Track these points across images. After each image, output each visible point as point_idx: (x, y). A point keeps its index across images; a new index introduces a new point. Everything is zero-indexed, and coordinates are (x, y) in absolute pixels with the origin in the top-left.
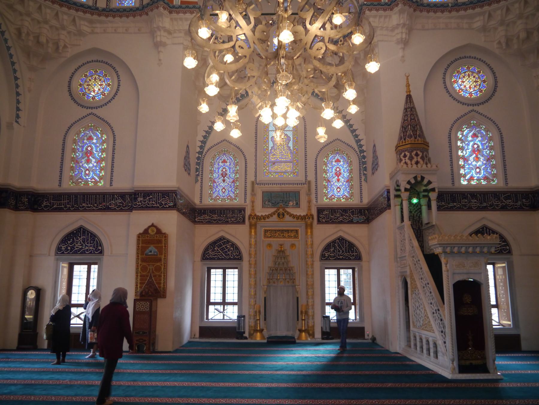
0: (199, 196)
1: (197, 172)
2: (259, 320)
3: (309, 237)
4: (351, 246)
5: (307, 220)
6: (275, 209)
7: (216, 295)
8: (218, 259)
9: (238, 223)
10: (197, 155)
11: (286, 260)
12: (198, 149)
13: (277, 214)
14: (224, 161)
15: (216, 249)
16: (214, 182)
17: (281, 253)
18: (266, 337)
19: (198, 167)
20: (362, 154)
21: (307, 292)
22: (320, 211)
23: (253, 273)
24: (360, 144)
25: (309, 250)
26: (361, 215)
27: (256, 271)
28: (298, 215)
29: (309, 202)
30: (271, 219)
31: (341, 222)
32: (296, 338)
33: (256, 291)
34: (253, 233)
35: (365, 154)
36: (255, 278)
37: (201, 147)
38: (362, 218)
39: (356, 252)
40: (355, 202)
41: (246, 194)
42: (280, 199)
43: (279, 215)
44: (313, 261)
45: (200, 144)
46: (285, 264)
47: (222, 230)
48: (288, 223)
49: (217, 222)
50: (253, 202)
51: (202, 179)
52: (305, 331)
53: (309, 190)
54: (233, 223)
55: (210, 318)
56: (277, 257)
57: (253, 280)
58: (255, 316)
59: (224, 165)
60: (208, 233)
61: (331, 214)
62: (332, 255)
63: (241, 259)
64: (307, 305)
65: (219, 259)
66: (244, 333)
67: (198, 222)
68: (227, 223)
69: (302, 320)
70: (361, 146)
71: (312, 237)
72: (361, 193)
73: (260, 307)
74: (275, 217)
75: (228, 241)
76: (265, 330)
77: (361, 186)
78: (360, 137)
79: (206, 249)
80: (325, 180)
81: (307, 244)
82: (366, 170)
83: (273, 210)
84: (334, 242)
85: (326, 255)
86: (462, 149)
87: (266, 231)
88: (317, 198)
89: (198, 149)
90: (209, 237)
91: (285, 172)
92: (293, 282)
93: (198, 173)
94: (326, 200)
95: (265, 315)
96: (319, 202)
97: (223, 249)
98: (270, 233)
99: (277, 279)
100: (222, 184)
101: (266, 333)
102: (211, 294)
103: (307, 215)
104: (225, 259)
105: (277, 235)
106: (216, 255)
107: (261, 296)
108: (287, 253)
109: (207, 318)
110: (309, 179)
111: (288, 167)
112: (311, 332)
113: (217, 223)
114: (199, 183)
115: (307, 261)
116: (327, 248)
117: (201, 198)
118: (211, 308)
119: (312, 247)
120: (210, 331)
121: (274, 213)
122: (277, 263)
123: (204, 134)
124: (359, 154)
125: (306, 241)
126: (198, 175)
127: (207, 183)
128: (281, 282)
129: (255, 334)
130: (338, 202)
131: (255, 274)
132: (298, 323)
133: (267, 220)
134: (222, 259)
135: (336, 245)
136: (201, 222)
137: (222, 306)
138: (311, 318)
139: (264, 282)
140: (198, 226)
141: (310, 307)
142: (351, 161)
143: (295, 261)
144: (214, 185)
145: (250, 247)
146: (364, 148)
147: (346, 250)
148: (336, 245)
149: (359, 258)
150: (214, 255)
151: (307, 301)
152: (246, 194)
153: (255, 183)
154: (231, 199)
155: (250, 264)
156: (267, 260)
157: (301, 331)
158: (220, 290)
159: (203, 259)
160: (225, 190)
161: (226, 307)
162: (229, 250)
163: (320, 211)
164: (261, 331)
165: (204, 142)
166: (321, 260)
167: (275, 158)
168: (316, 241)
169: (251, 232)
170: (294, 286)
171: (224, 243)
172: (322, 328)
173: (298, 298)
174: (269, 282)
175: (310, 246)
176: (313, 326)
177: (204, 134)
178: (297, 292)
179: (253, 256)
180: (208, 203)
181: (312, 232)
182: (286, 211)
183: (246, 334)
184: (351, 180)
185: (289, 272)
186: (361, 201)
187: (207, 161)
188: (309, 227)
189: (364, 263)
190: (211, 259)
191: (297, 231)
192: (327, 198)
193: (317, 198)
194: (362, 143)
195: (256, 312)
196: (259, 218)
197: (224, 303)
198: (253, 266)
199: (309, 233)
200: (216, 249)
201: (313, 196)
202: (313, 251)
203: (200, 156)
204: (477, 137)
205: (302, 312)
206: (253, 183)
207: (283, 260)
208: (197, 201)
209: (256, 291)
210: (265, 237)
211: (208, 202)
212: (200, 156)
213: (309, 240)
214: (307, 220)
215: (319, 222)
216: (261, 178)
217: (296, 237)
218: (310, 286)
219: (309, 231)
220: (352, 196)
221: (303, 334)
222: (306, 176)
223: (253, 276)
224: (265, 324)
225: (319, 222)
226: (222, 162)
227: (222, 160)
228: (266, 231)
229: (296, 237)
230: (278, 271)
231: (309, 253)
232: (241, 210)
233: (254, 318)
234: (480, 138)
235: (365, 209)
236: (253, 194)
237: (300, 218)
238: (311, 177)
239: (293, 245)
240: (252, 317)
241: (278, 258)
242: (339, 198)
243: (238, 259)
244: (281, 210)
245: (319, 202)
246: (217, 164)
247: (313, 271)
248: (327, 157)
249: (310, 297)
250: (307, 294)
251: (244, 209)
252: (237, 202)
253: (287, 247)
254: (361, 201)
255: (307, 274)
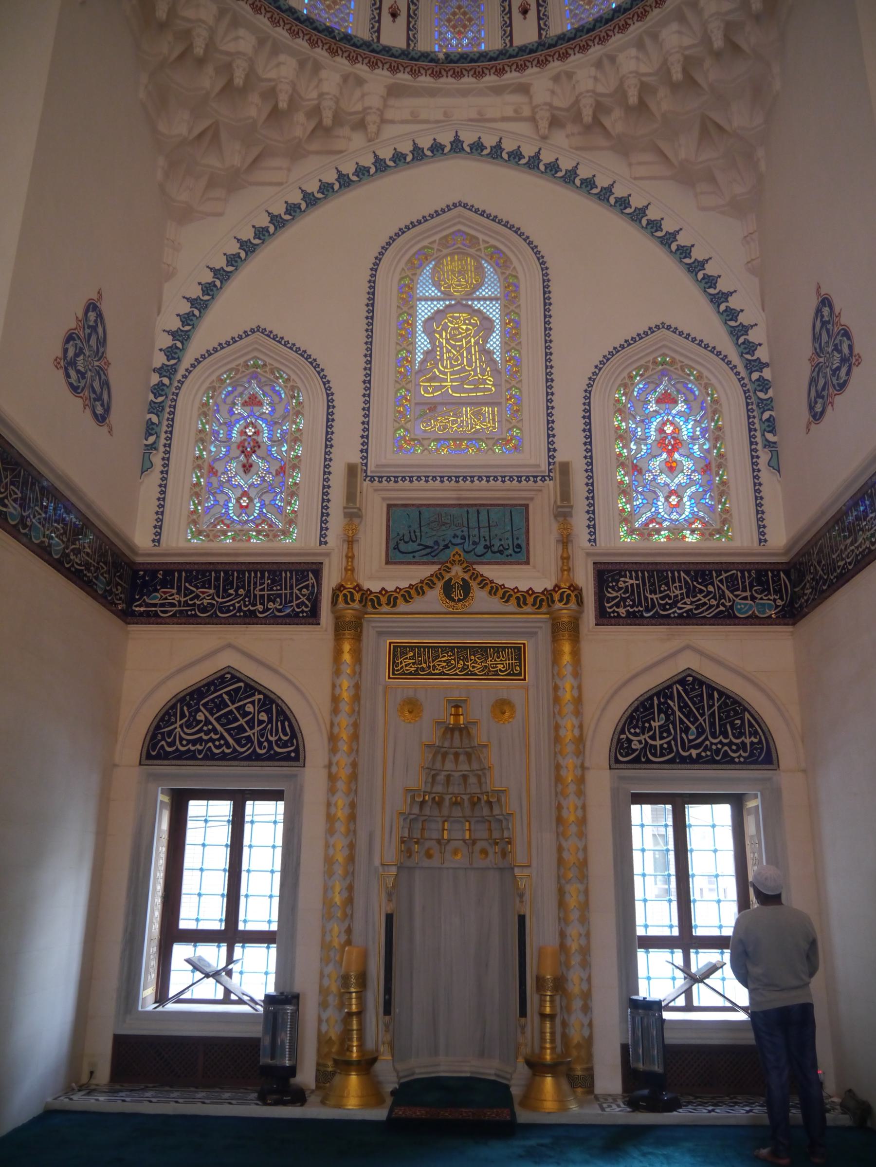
0: (150, 519)
1: (148, 434)
2: (360, 1014)
3: (568, 670)
4: (732, 712)
5: (558, 605)
6: (434, 568)
7: (201, 907)
8: (206, 758)
9: (294, 619)
10: (155, 379)
11: (475, 766)
12: (160, 359)
13: (440, 585)
14: (253, 401)
15: (200, 717)
16: (213, 472)
17: (456, 737)
18: (389, 1088)
19: (155, 419)
20: (755, 376)
21: (561, 892)
22: (606, 574)
23: (341, 813)
24: (746, 342)
25: (568, 723)
26: (766, 590)
27: (353, 805)
28: (523, 587)
29: (565, 541)
30: (418, 604)
31: (688, 619)
32: (516, 1091)
33: (350, 888)
34: (347, 657)
35: (767, 373)
36: (351, 832)
37: (172, 353)
38: (769, 605)
39: (756, 734)
40: (739, 541)
41: (325, 514)
42: (456, 535)
43: (448, 590)
44: (583, 767)
45: (167, 341)
46: (472, 780)
47: (230, 646)
48: (482, 620)
49: (211, 615)
50: (351, 541)
51: (166, 461)
52: (552, 1069)
53: (565, 494)
54: (275, 620)
55: (173, 990)
56: (439, 753)
57: (340, 842)
58: (343, 995)
59: (251, 414)
60: (170, 658)
61: (643, 590)
62: (658, 743)
63: (297, 758)
64: (563, 947)
65: (210, 757)
66: (292, 1071)
67: (141, 614)
68: (250, 618)
69: (543, 1016)
70: (750, 348)
71: (577, 674)
72: (760, 512)
73: (364, 956)
74: (434, 598)
75: (251, 688)
76: (386, 1057)
77: (757, 485)
78: (742, 319)
79: (165, 717)
80: (623, 465)
81: (557, 700)
82: (773, 431)
83: (426, 571)
84: (663, 692)
85: (635, 745)
86: (624, 437)
87: (398, 651)
88: (592, 528)
89: (160, 359)
90: (180, 671)
91: (475, 438)
92: (504, 854)
93: (152, 439)
94: (625, 539)
95: (388, 990)
96: (603, 543)
97: (228, 719)
98: (414, 658)
99: (439, 842)
100: (239, 480)
101: (389, 1073)
102: (184, 900)
103: (557, 587)
104: (235, 757)
105: (441, 664)
106: (200, 740)
107: (373, 909)
108: (481, 736)
109: (162, 996)
110: (560, 457)
111: (488, 421)
112: (579, 1070)
113: (213, 620)
114: (154, 477)
115: (558, 767)
116: (639, 715)
117: (158, 528)
118: (181, 952)
119: (578, 713)
120: (159, 1056)
121: (430, 583)
122: (441, 777)
123: (186, 308)
124: (744, 373)
125: (556, 688)
126: (153, 447)
127: (183, 475)
128: (455, 852)
129: (337, 1078)
130: (673, 544)
131: (352, 817)
132: (523, 1027)
133: (402, 607)
134: (224, 757)
135: (674, 705)
136: (151, 617)
137: (224, 948)
138: (577, 1004)
139: (385, 850)
140: (135, 629)
141: (575, 960)
142: (715, 401)
143: (513, 767)
144: (209, 484)
145: (335, 711)
146: (762, 354)
147: (712, 725)
148: (674, 705)
149: (763, 755)
150: (194, 742)
151: (562, 935)
152: (325, 514)
153: (360, 475)
154: (272, 534)
155: (332, 778)
156: (398, 762)
157: (537, 1067)
158: (218, 883)
159: (149, 757)
160: (251, 500)
161: (238, 949)
162: (251, 724)
163: (606, 574)
164: (367, 1065)
165: (182, 336)
166: (615, 762)
167: (436, 389)
168: (596, 689)
169: (338, 653)
170: (507, 871)
171: (234, 696)
172: (625, 1048)
173: (522, 919)
174: (409, 853)
175: (569, 708)
176: (589, 1042)
177: (186, 308)
178: (521, 896)
179: (344, 747)
180: (182, 544)
181: (576, 653)
182: (475, 576)
183: (306, 1077)
184: (719, 466)
185: (486, 811)
186: (762, 541)
187: (189, 399)
188: (566, 635)
189: (787, 778)
190: (180, 756)
191: (518, 652)
192: (631, 532)
193: (592, 528)
194: (753, 336)
195: (345, 980)
196: (370, 600)
197: (231, 934)
198: (341, 785)
199: (566, 658)
200: (200, 717)
201: (579, 521)
202: (581, 727)
203: (166, 381)
204: (675, 402)
205: (540, 982)
206: (352, 470)
207: (465, 767)
208: (141, 538)
209: (350, 888)
210: (396, 671)
211: (183, 541)
212: (166, 381)
213: (568, 684)
214: (558, 605)
215: (604, 617)
216: (383, 455)
217: (515, 674)
218: (572, 870)
219: (567, 648)
220: (724, 522)
221: (549, 1081)
222: (551, 450)
223: (341, 827)
224: (387, 1026)
225: (604, 617)
226: (245, 404)
227: (246, 397)
228: (398, 651)
229: (515, 674)
230: (445, 811)
231: (568, 734)
232: (308, 572)
233: (342, 1005)
234: (681, 407)
235: (775, 569)
236: (354, 514)
237: (530, 600)
238: (570, 450)
239: (502, 706)
240: (333, 1000)
241: (444, 756)
242: (676, 530)
243: (287, 758)
244: (457, 571)
245: (603, 543)
246: (224, 409)
247: (584, 807)
248: (625, 386)
249: (574, 915)
250: (562, 904)
251: (317, 570)
252: (296, 542)
253: (479, 711)
254: (762, 541)
255: (559, 820)
